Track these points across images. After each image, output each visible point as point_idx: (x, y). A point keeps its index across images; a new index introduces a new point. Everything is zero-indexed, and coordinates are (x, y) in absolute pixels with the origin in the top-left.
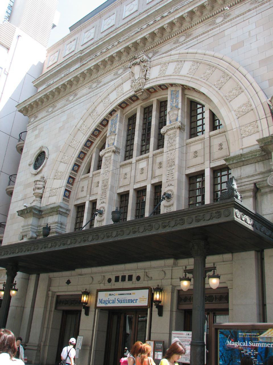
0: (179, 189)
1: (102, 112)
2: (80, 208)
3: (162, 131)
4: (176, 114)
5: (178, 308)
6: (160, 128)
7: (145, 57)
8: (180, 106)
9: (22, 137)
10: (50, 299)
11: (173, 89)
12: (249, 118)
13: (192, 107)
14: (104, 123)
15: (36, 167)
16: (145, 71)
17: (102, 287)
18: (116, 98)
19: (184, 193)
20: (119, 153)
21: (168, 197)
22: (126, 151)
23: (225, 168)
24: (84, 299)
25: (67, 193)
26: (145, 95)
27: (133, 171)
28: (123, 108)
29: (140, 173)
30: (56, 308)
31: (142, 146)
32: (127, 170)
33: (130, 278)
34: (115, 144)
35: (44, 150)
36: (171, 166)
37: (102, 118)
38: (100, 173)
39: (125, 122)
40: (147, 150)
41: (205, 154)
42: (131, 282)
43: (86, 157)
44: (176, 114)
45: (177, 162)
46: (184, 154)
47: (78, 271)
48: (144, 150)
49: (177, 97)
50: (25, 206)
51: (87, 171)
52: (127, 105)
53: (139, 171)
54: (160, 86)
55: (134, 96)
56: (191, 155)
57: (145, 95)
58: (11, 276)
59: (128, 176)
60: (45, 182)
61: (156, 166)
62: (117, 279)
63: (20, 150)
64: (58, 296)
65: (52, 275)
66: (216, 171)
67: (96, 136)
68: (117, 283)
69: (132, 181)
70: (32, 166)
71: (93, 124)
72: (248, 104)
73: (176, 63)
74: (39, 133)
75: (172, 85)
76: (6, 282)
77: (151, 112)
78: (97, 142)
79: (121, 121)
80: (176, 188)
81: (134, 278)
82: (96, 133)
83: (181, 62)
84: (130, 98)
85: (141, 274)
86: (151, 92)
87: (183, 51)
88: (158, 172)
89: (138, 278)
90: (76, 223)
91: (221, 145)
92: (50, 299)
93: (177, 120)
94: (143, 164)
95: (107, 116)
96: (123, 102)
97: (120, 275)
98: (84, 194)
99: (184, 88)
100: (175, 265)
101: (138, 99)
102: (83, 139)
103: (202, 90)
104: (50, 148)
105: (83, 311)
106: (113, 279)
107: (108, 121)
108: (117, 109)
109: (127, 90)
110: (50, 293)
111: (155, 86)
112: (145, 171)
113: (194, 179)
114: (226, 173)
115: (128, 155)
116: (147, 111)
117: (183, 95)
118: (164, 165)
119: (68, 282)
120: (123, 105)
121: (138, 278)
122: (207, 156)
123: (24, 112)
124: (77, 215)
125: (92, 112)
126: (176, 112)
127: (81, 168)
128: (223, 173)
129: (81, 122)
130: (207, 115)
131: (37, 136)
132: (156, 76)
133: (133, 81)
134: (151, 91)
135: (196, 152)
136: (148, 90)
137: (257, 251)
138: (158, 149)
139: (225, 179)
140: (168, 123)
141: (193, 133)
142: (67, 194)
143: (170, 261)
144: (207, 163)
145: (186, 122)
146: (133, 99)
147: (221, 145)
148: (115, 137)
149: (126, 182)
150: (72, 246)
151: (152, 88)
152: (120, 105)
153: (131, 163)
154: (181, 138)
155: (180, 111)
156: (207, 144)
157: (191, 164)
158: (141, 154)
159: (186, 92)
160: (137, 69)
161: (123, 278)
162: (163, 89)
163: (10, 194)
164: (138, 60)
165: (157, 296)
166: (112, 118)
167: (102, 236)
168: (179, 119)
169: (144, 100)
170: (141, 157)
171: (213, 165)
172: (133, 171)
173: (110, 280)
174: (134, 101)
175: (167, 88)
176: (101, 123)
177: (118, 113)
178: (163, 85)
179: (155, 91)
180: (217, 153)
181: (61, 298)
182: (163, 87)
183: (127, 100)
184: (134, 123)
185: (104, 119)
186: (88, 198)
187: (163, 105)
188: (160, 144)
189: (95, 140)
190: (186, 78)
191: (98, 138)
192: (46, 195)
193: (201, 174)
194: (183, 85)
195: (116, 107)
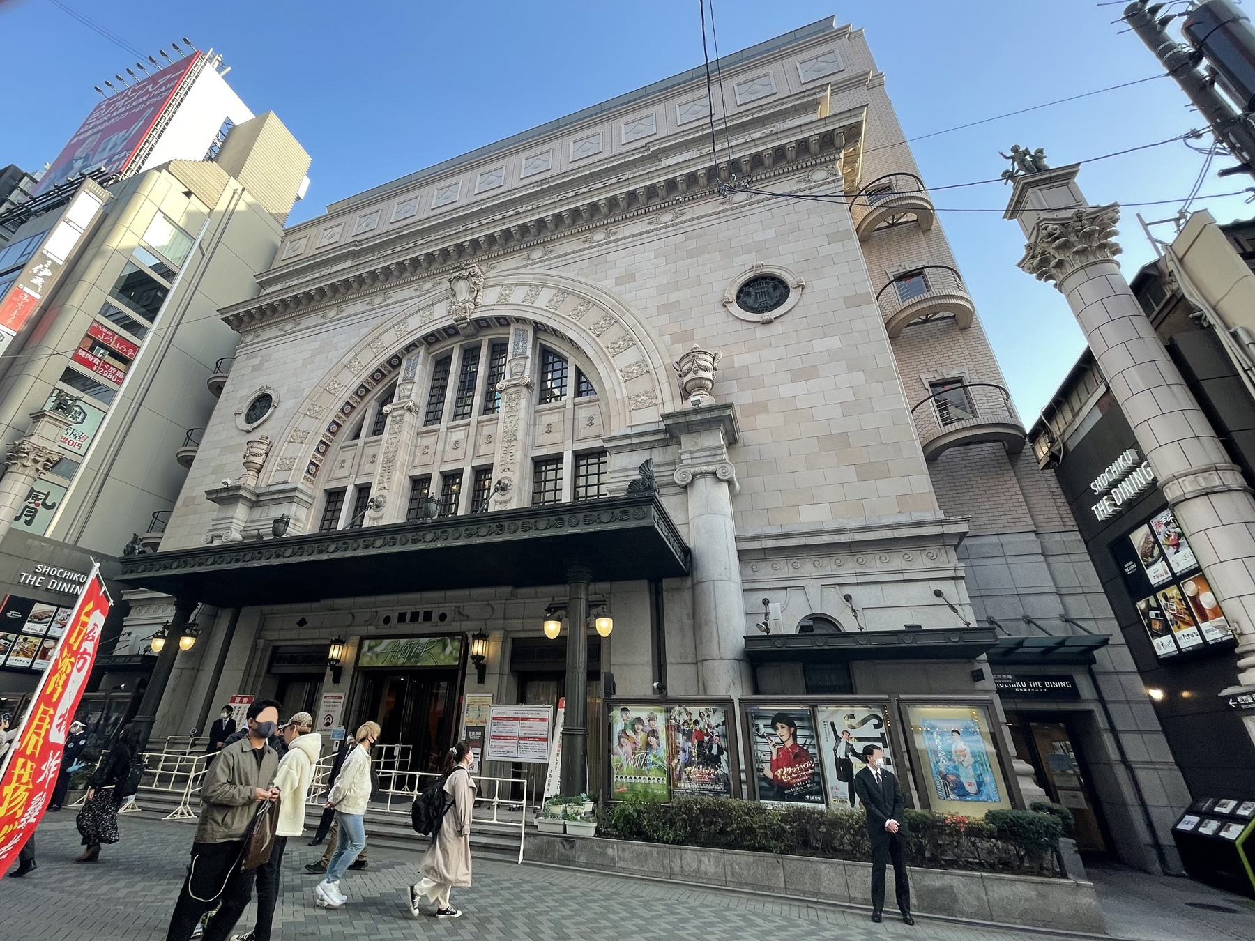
0: (522, 477)
1: (392, 343)
2: (334, 496)
3: (385, 409)
4: (520, 364)
5: (511, 669)
6: (382, 405)
7: (477, 269)
8: (529, 353)
9: (224, 363)
10: (259, 654)
11: (520, 326)
12: (643, 385)
13: (547, 358)
14: (394, 363)
15: (249, 419)
16: (475, 291)
17: (372, 630)
18: (418, 326)
19: (528, 485)
20: (417, 413)
21: (502, 488)
22: (428, 412)
23: (600, 453)
24: (335, 652)
25: (313, 469)
26: (470, 330)
27: (440, 445)
28: (430, 344)
29: (454, 447)
30: (268, 671)
31: (457, 407)
32: (429, 440)
33: (415, 617)
34: (412, 397)
35: (268, 391)
36: (511, 441)
37: (392, 352)
38: (438, 430)
39: (430, 366)
40: (438, 420)
41: (565, 427)
42: (428, 624)
43: (354, 413)
44: (520, 364)
45: (520, 435)
46: (532, 425)
47: (326, 602)
48: (461, 412)
49: (524, 341)
50: (225, 483)
51: (352, 435)
52: (437, 340)
53: (450, 446)
54: (498, 318)
55: (452, 327)
56: (542, 429)
57: (470, 330)
58: (184, 610)
59: (430, 451)
60: (270, 446)
61: (483, 439)
62: (402, 618)
63: (217, 388)
64: (275, 649)
65: (266, 608)
66: (578, 456)
67: (377, 382)
68: (401, 625)
69: (470, 453)
70: (243, 417)
71: (372, 361)
72: (641, 363)
73: (527, 288)
74: (262, 363)
75: (518, 320)
76: (171, 620)
77: (477, 357)
78: (378, 390)
79: (424, 365)
80: (517, 475)
81: (435, 617)
82: (378, 376)
83: (537, 286)
84: (445, 329)
85: (447, 608)
86: (481, 327)
87: (542, 271)
88: (484, 449)
89: (443, 617)
90: (323, 521)
91: (591, 418)
92: (259, 654)
93: (522, 373)
94: (459, 435)
95: (400, 351)
96: (432, 334)
97: (409, 610)
98: (345, 472)
99: (539, 328)
100: (513, 596)
101: (457, 333)
102: (351, 382)
103: (570, 334)
104: (283, 391)
105: (329, 674)
106: (395, 619)
107: (400, 361)
108: (421, 344)
109: (440, 316)
110: (261, 642)
111: (490, 317)
112: (462, 446)
113: (544, 464)
114: (554, 467)
115: (433, 416)
116: (470, 355)
117: (535, 339)
118: (380, 457)
119: (302, 623)
120: (430, 340)
121: (443, 617)
122: (569, 433)
123: (235, 323)
124: (327, 507)
125: (373, 341)
126: (522, 362)
127: (342, 430)
128: (590, 461)
129: (352, 354)
130: (571, 373)
131: (255, 368)
132: (490, 303)
133: (452, 303)
134: (482, 324)
135: (549, 425)
136: (477, 321)
137: (650, 581)
138: (374, 434)
139: (551, 475)
140: (395, 400)
141: (544, 396)
142: (314, 469)
143: (508, 589)
144: (568, 443)
145: (536, 380)
146: (450, 332)
147: (591, 418)
148: (415, 386)
149: (427, 459)
150: (339, 555)
151: (484, 319)
152: (425, 338)
153: (438, 430)
154: (529, 402)
155: (529, 361)
156: (569, 415)
157: (539, 442)
158: (454, 420)
159: (540, 335)
160: (462, 286)
161: (415, 617)
162: (501, 325)
163: (187, 462)
164: (466, 273)
165: (478, 648)
166: (409, 356)
167: (404, 540)
168: (527, 372)
169: (467, 337)
170: (457, 423)
171: (577, 447)
172: (440, 445)
173: (387, 620)
174: (450, 336)
175: (509, 325)
176: (389, 362)
177: (422, 351)
178: (504, 318)
179: (488, 326)
180: (584, 431)
181: (281, 650)
182: (504, 322)
183: (438, 331)
184: (447, 371)
185: (396, 356)
186: (351, 480)
187: (498, 349)
188: (489, 406)
189: (373, 387)
190: (543, 313)
191: (380, 386)
192: (272, 465)
193: (459, 474)
194: (536, 323)
195: (418, 340)
